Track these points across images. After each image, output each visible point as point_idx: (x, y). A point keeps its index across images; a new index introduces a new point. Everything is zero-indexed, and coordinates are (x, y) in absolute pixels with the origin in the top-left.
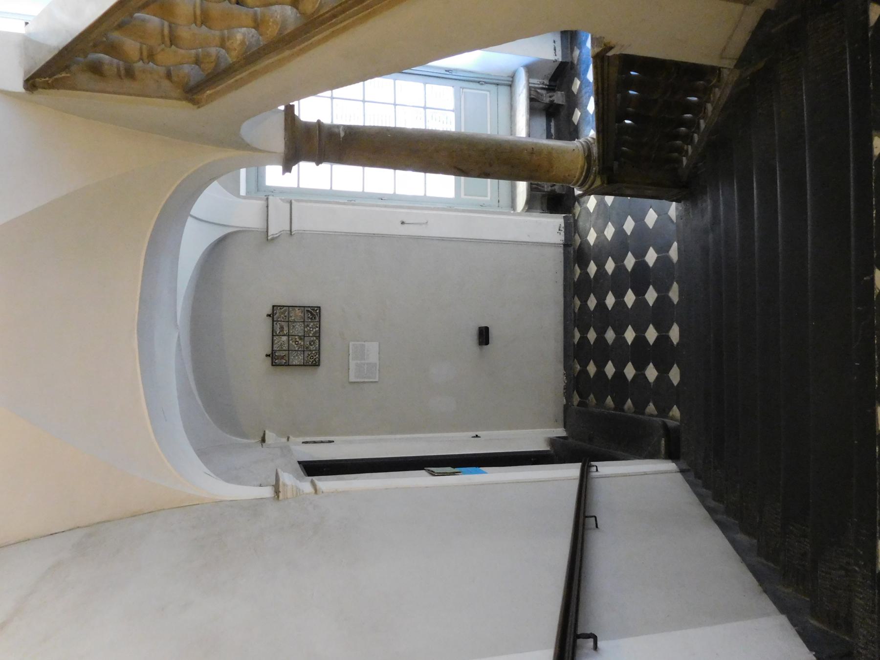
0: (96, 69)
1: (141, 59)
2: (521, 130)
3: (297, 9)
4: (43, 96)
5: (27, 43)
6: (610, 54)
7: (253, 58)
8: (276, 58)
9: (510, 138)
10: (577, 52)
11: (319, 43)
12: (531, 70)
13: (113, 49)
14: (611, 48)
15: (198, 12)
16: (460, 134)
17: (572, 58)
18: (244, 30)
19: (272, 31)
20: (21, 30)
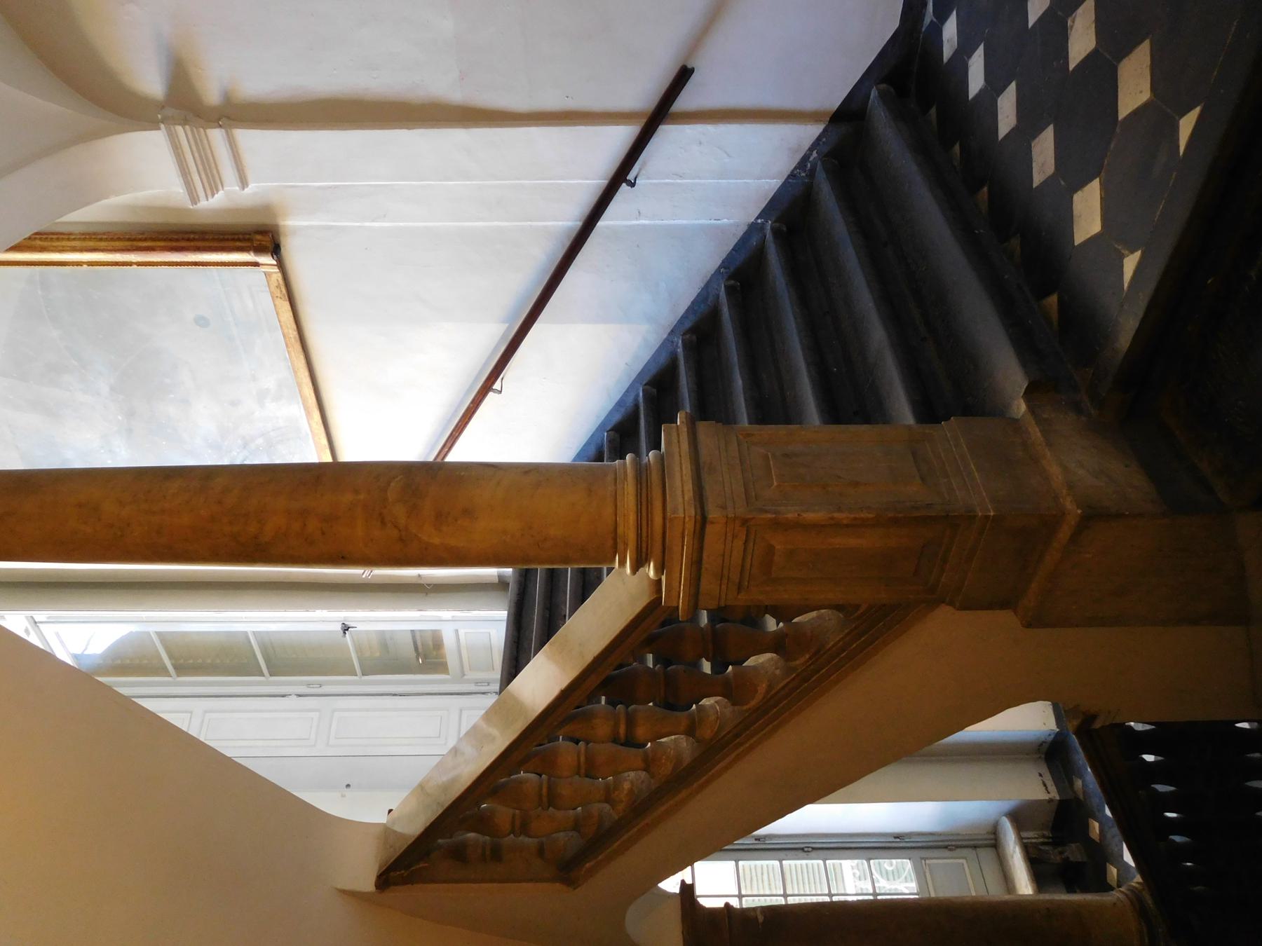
0: (459, 854)
1: (513, 832)
2: (1024, 886)
3: (694, 737)
4: (398, 894)
5: (386, 833)
6: (1097, 725)
7: (643, 809)
8: (671, 802)
9: (1007, 897)
10: (1078, 783)
11: (726, 768)
12: (1019, 817)
13: (482, 823)
14: (1094, 717)
15: (582, 759)
16: (930, 899)
17: (1075, 792)
18: (632, 774)
19: (666, 769)
20: (383, 819)
